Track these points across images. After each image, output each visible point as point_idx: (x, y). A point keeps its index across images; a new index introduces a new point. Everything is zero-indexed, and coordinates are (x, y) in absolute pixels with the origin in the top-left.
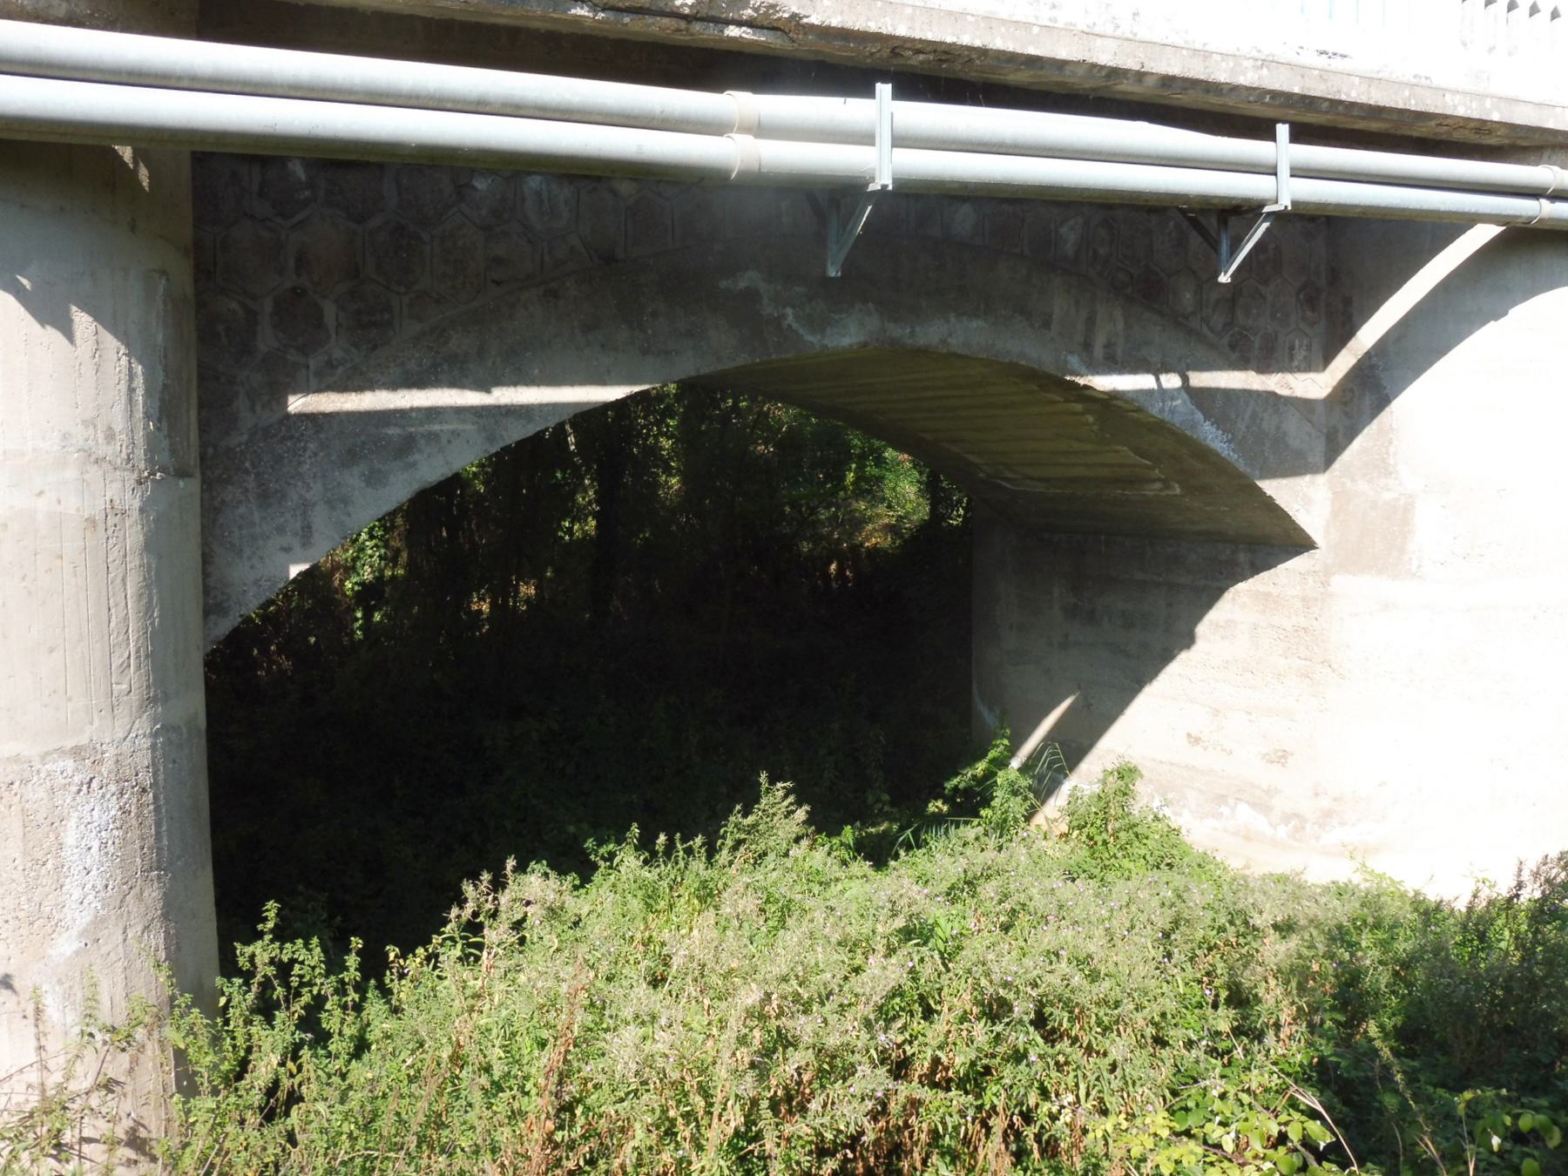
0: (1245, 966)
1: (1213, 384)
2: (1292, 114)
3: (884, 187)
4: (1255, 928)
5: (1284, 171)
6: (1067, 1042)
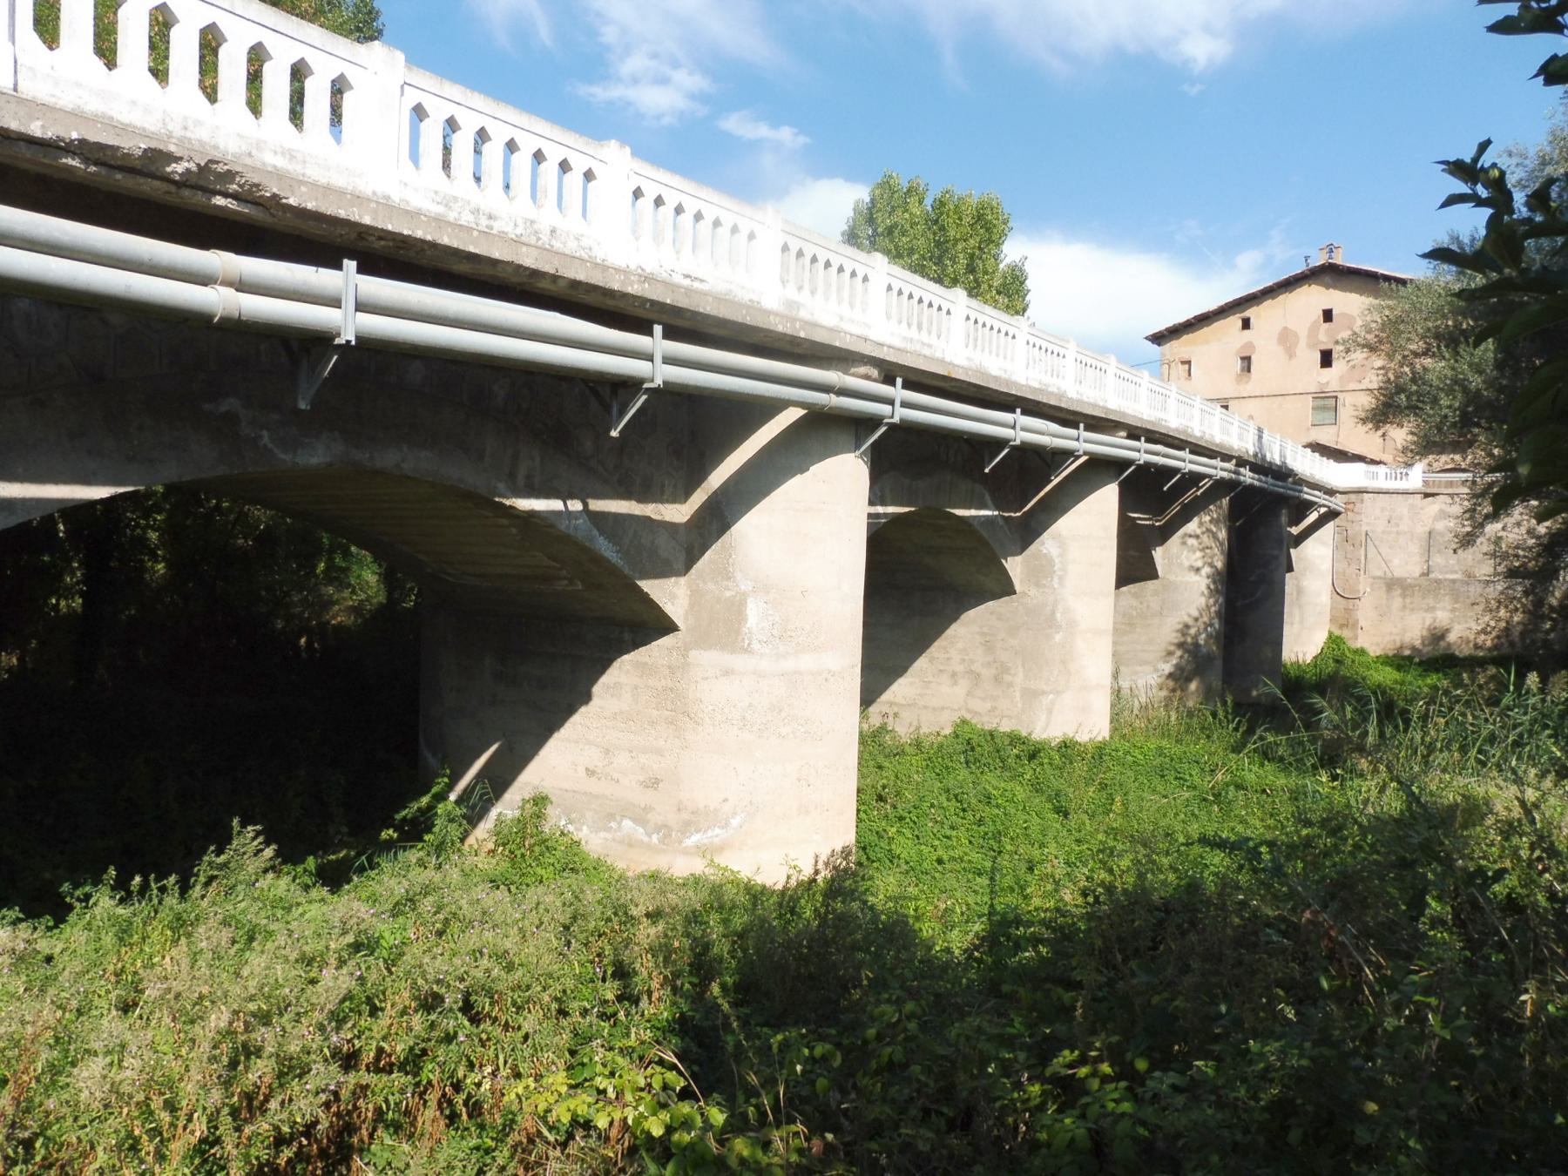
0: (626, 947)
1: (606, 509)
2: (665, 318)
3: (348, 342)
4: (632, 918)
5: (658, 358)
6: (489, 1022)
